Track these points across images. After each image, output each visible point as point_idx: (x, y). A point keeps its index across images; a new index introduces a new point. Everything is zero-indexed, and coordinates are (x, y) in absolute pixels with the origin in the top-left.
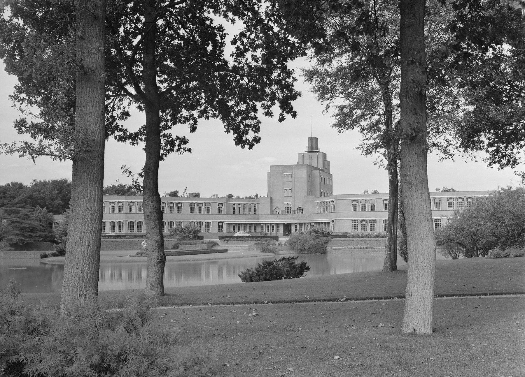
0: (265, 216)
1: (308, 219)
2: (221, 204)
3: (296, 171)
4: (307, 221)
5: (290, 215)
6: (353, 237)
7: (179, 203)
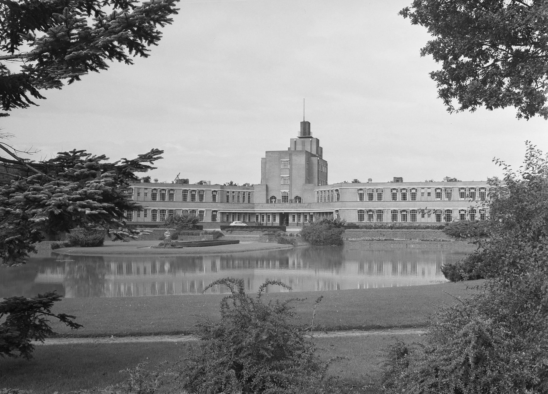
0: (260, 205)
1: (308, 208)
2: (215, 191)
3: (294, 158)
4: (306, 210)
5: (287, 204)
6: (391, 228)
7: (172, 190)
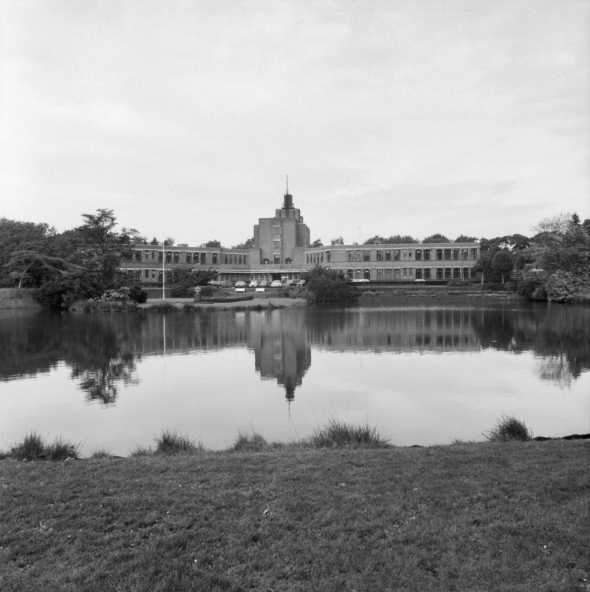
5: (229, 265)
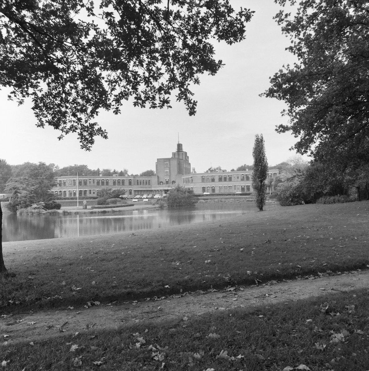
5: (139, 186)
